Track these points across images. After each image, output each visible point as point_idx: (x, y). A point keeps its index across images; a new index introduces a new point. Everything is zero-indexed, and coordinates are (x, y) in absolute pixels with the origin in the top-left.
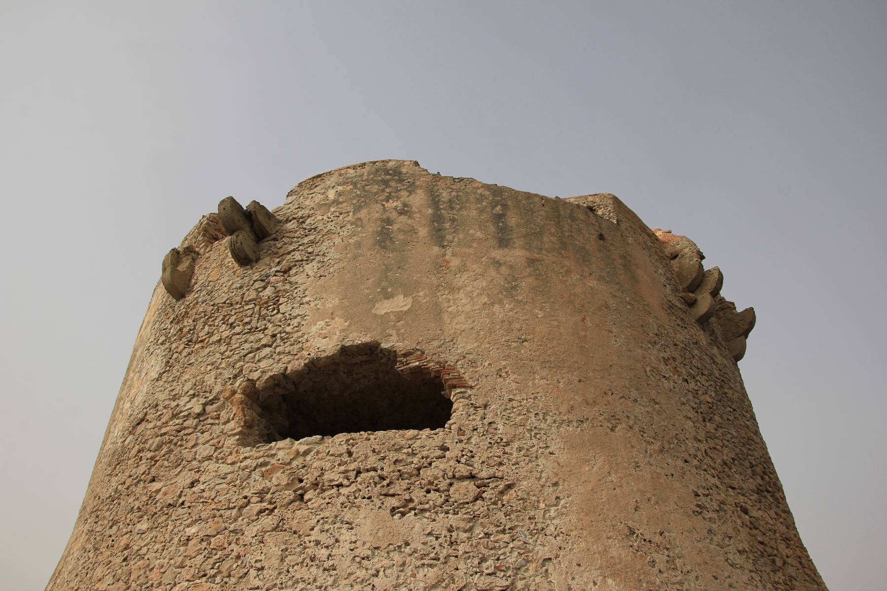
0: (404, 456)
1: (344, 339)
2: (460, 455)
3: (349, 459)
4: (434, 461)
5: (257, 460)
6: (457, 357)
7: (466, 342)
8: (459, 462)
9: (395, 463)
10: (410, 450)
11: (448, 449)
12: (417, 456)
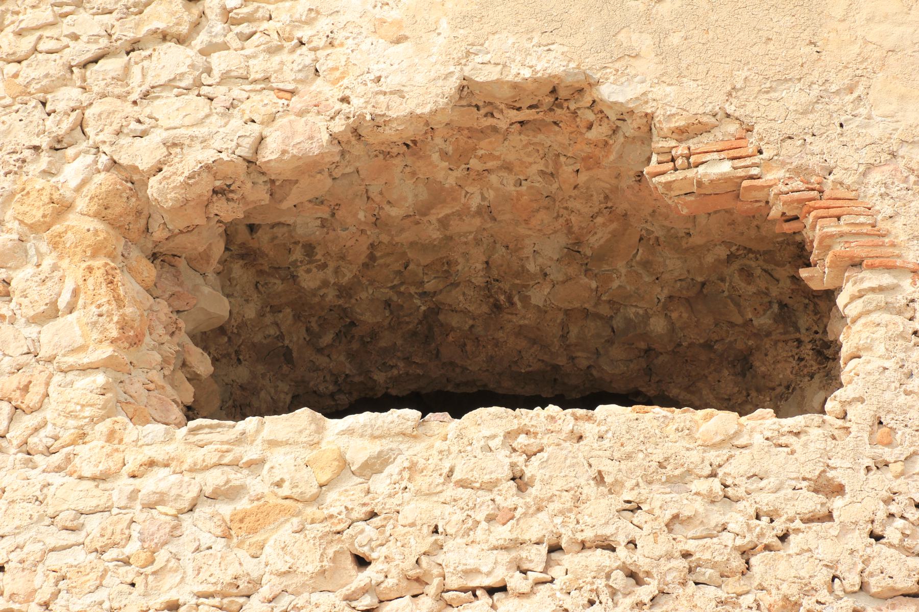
0: (699, 505)
1: (468, 54)
2: (881, 515)
3: (518, 501)
4: (797, 531)
5: (199, 477)
6: (866, 156)
7: (902, 97)
8: (877, 538)
9: (671, 524)
10: (716, 484)
11: (839, 490)
12: (740, 506)
